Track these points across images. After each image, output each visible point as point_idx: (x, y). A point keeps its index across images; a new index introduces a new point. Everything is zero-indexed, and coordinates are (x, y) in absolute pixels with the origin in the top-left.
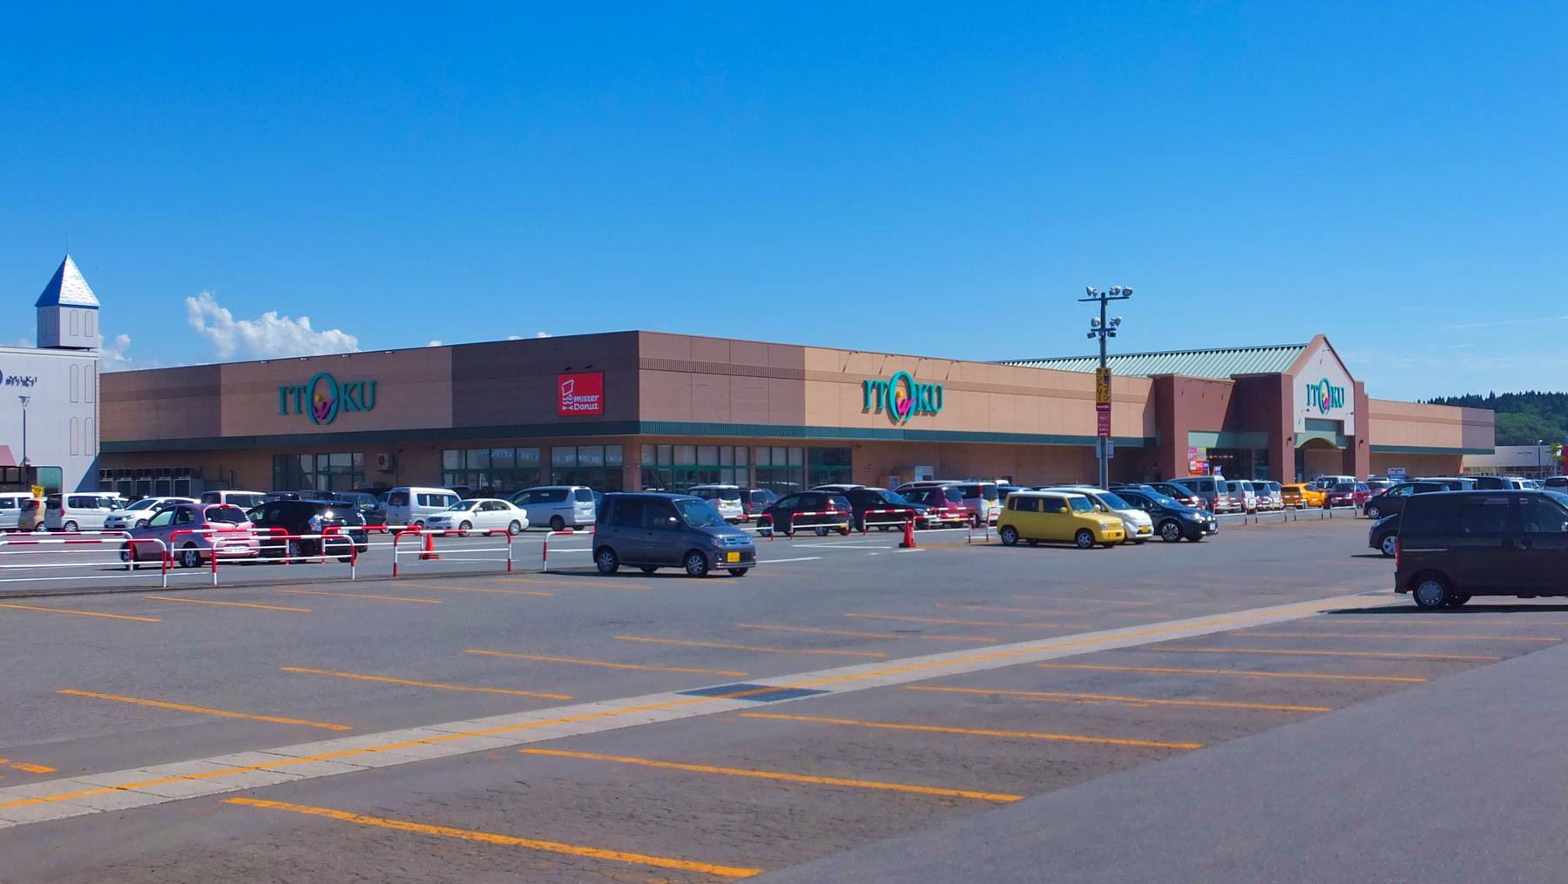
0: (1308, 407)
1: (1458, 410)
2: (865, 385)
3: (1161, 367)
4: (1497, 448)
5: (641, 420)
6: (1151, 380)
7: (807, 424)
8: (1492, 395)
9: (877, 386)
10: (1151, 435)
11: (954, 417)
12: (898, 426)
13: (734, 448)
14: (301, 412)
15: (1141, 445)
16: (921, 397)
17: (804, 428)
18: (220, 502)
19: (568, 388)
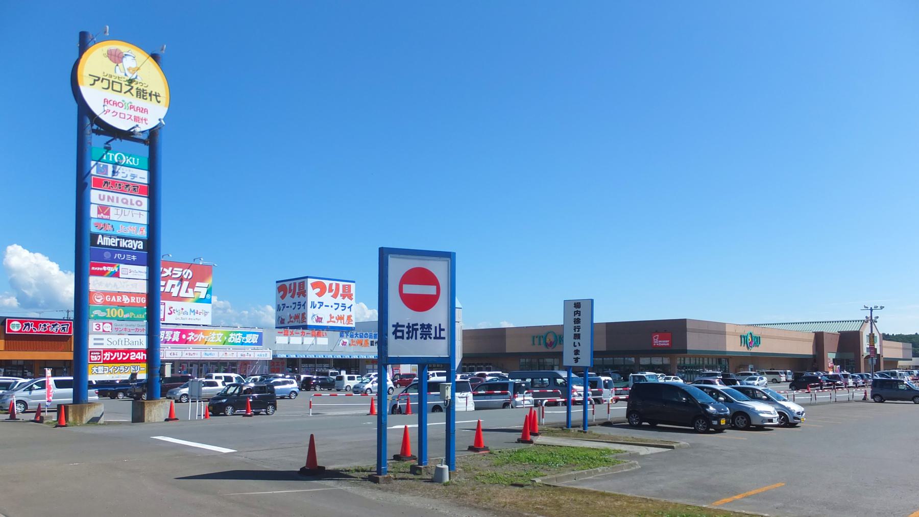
0: (330, 306)
1: (900, 345)
2: (741, 337)
3: (819, 328)
4: (913, 358)
5: (688, 349)
6: (814, 334)
7: (727, 350)
8: (893, 335)
9: (744, 337)
10: (815, 354)
11: (765, 347)
12: (749, 351)
13: (690, 358)
14: (540, 345)
15: (812, 357)
16: (757, 341)
17: (726, 352)
18: (232, 381)
19: (656, 338)
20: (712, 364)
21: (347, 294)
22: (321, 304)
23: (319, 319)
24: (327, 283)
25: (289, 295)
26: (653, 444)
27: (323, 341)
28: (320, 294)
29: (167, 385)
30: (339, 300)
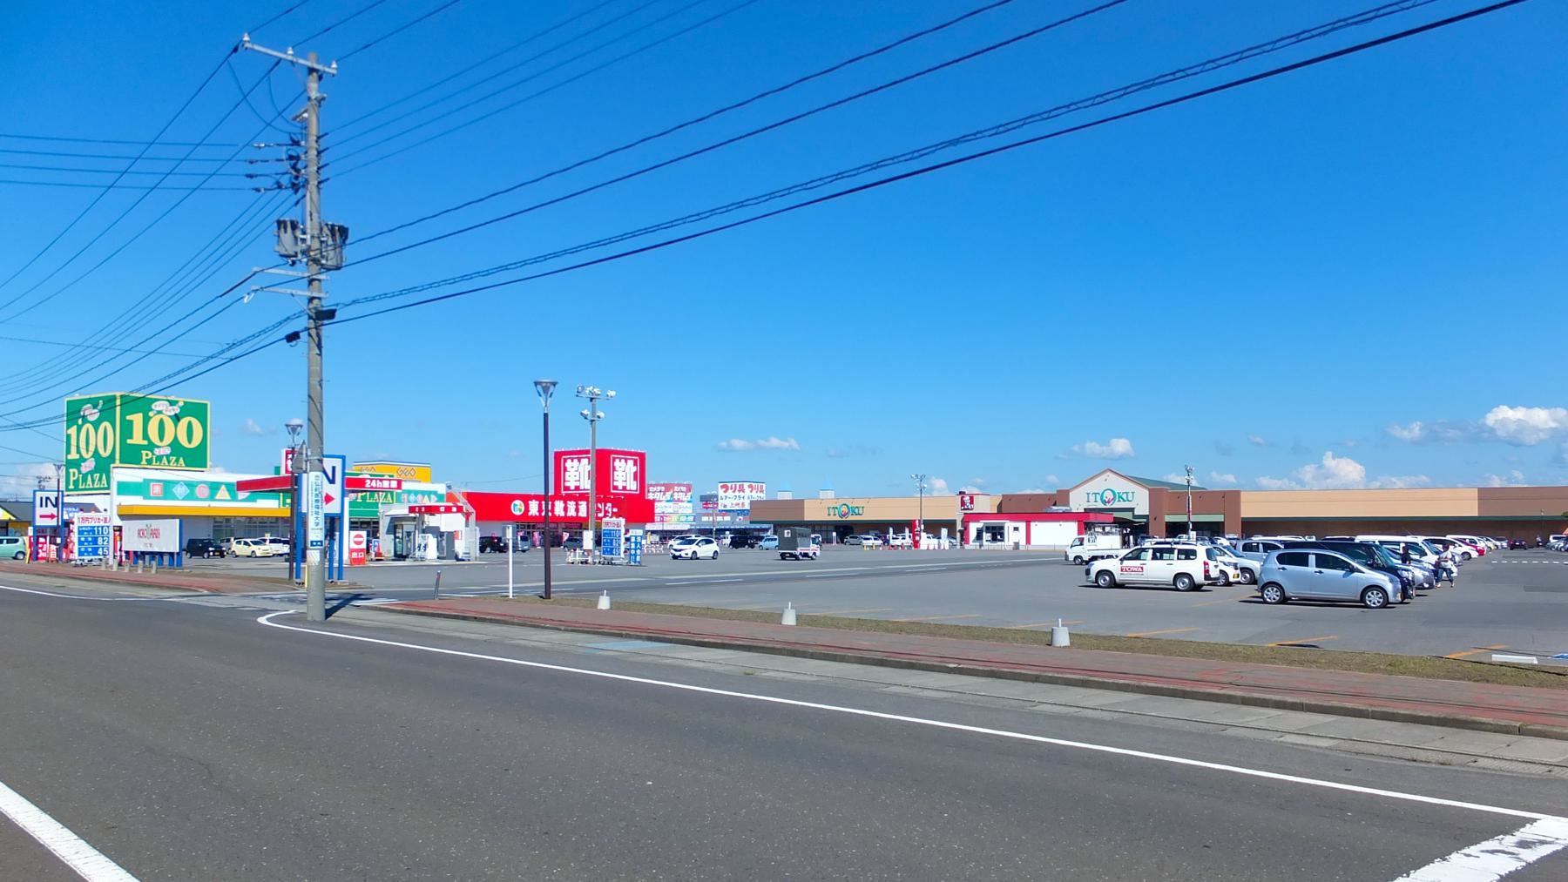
20: (577, 505)
21: (742, 490)
22: (726, 497)
23: (725, 506)
24: (729, 485)
25: (754, 491)
26: (1335, 703)
27: (727, 518)
28: (725, 492)
29: (1342, 758)
30: (737, 493)
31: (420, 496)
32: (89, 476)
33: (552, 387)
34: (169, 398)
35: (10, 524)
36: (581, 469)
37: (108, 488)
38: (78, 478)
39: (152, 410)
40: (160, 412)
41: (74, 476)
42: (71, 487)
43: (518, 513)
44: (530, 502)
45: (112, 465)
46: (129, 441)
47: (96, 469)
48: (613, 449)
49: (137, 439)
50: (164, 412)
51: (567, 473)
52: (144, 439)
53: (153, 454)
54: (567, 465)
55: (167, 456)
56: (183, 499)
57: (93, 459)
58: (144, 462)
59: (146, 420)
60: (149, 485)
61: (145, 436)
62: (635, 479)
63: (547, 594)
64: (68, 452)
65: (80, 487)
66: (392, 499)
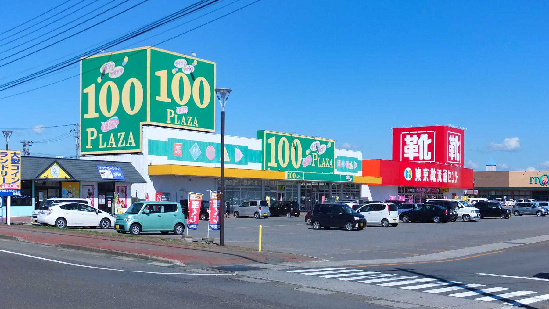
31: (348, 162)
32: (112, 137)
33: (228, 93)
34: (187, 57)
35: (63, 184)
36: (420, 142)
37: (137, 147)
38: (98, 137)
39: (175, 67)
40: (180, 70)
41: (92, 136)
42: (89, 146)
43: (408, 179)
44: (416, 169)
45: (141, 123)
46: (158, 98)
47: (120, 128)
48: (404, 127)
49: (163, 97)
50: (183, 70)
51: (406, 147)
52: (168, 97)
53: (175, 113)
54: (406, 139)
55: (186, 115)
56: (197, 161)
57: (117, 117)
58: (168, 121)
59: (170, 77)
60: (172, 144)
61: (170, 95)
62: (459, 153)
63: (222, 243)
64: (85, 110)
65: (100, 147)
66: (333, 166)
